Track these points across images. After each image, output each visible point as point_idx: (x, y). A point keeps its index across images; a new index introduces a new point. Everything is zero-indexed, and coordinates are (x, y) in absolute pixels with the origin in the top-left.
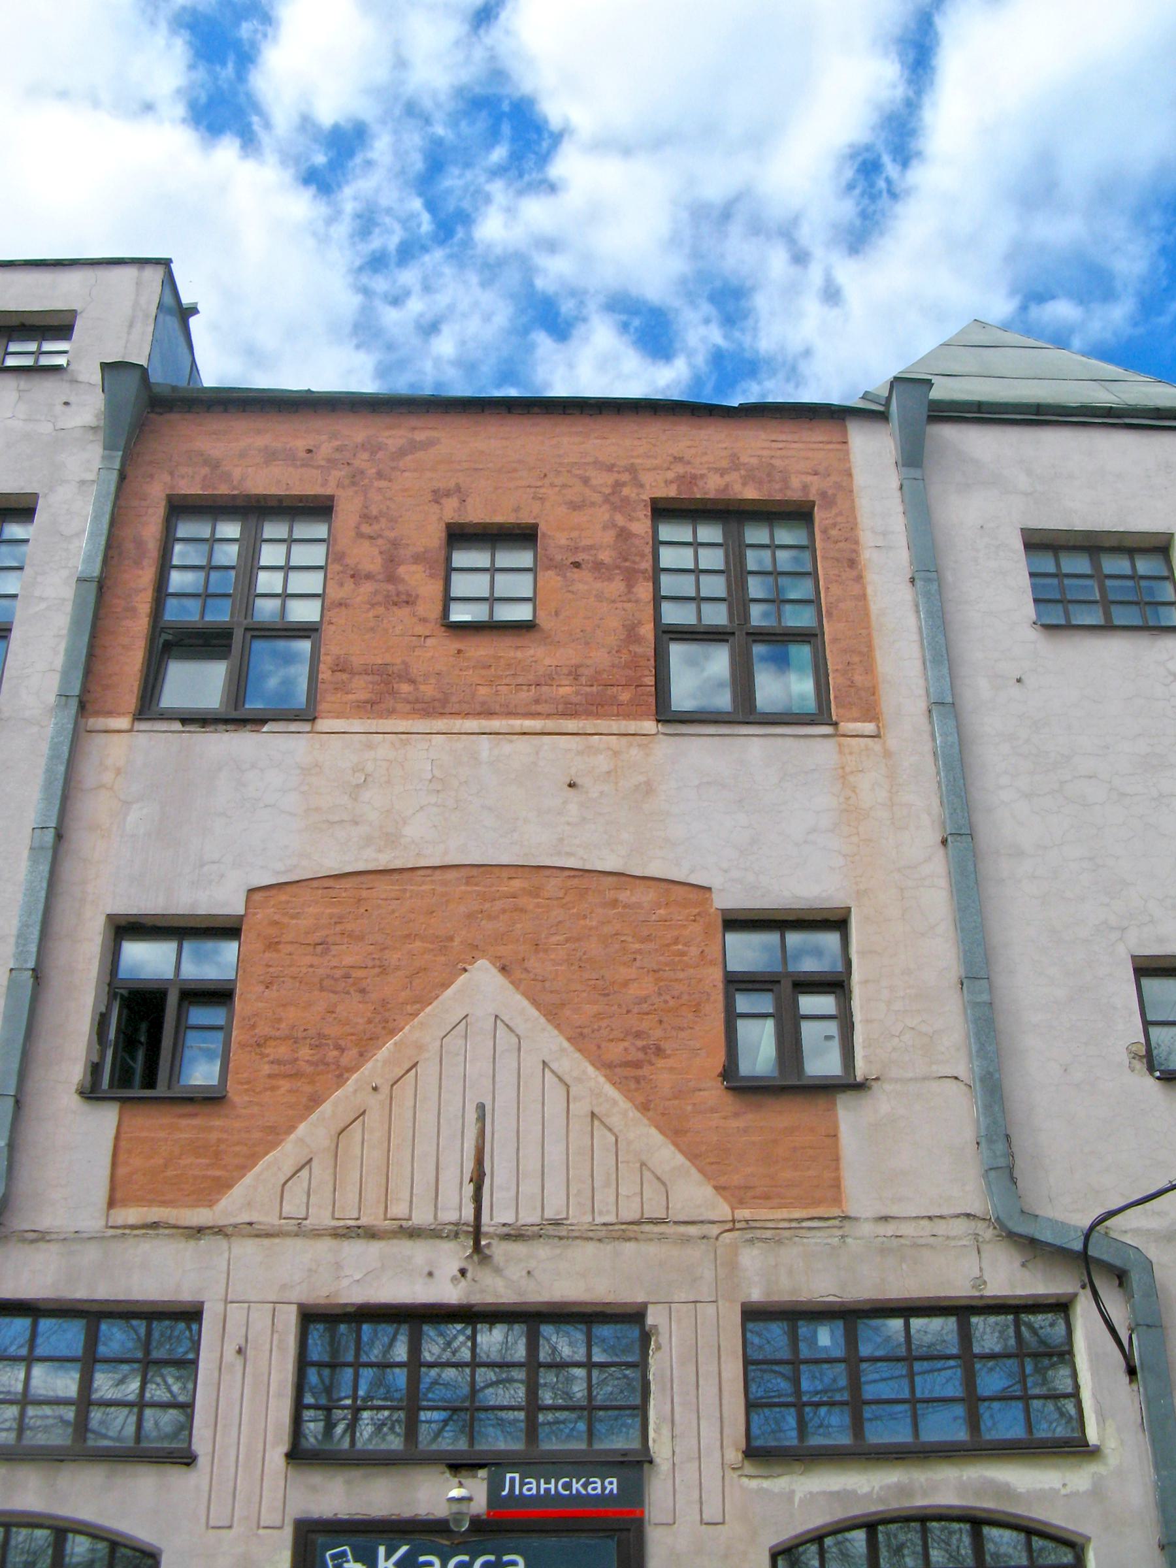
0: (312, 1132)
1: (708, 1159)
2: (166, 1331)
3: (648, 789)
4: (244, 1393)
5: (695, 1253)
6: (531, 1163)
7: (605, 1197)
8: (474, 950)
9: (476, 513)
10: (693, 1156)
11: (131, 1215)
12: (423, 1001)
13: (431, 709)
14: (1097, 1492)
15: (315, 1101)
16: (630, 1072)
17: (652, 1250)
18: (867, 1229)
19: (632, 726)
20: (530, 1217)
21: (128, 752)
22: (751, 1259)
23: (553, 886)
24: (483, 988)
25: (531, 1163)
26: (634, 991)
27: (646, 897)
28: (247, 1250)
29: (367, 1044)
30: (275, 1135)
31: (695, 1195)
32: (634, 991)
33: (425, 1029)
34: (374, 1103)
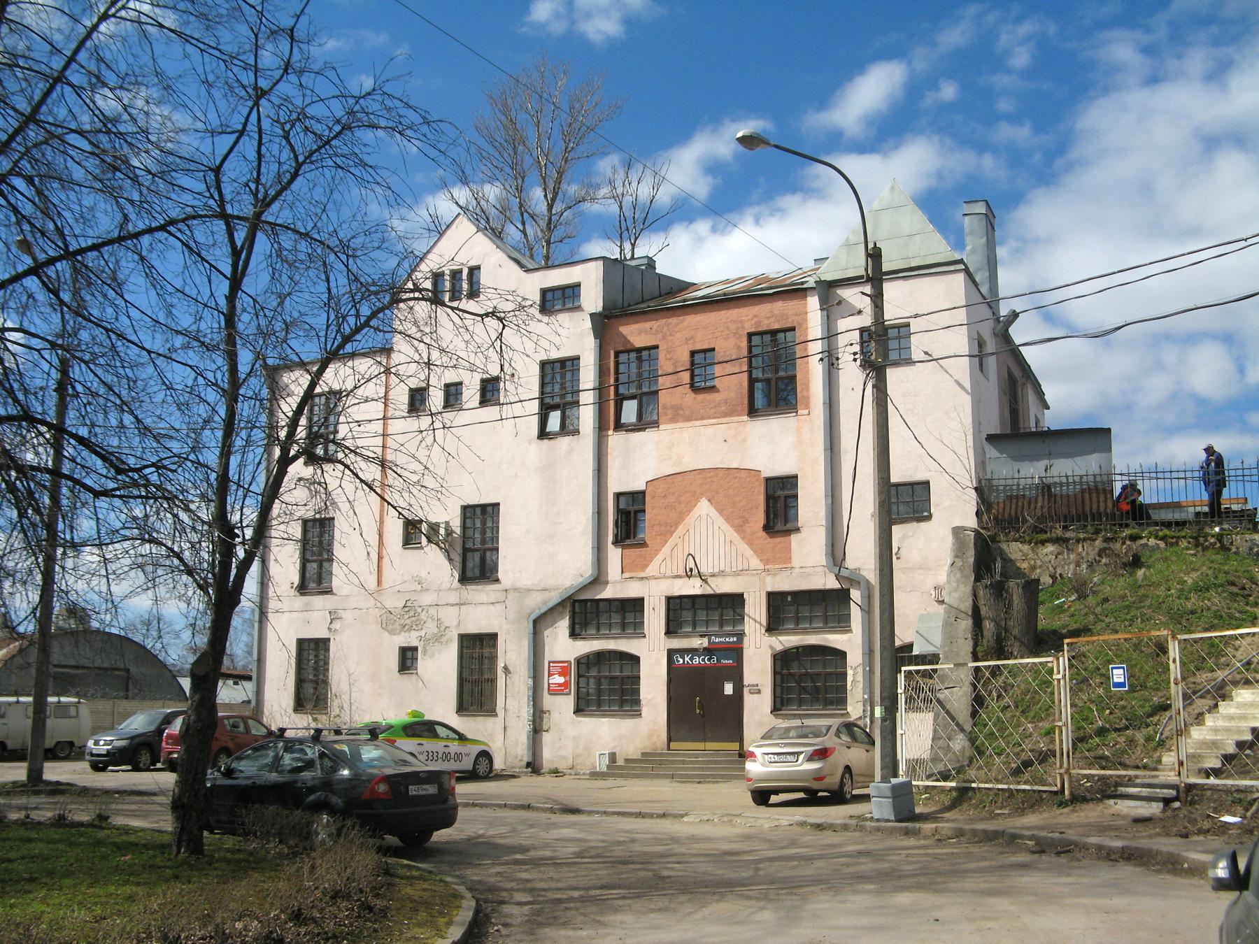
0: (665, 550)
1: (758, 552)
2: (636, 605)
3: (744, 440)
4: (655, 618)
5: (756, 578)
6: (716, 556)
7: (734, 564)
8: (702, 495)
9: (698, 347)
10: (755, 551)
11: (627, 575)
12: (690, 511)
13: (689, 419)
14: (849, 640)
15: (666, 542)
16: (739, 529)
17: (745, 578)
18: (797, 570)
19: (740, 418)
20: (716, 570)
21: (615, 440)
22: (769, 579)
23: (721, 473)
24: (704, 507)
25: (710, 548)
26: (742, 504)
27: (744, 474)
28: (653, 582)
29: (677, 524)
30: (657, 551)
31: (756, 563)
32: (742, 504)
33: (690, 520)
34: (680, 541)
